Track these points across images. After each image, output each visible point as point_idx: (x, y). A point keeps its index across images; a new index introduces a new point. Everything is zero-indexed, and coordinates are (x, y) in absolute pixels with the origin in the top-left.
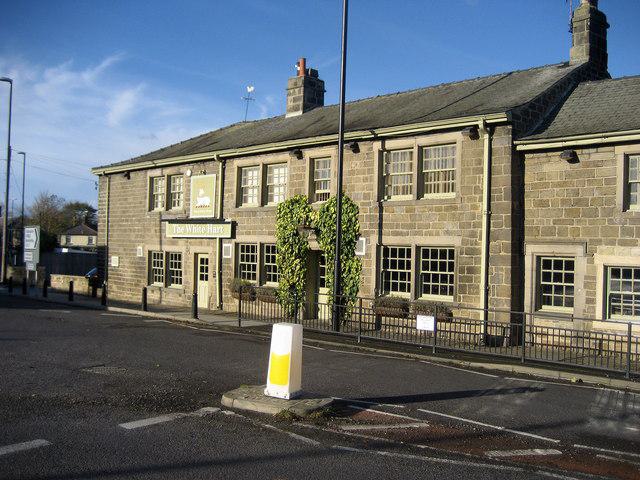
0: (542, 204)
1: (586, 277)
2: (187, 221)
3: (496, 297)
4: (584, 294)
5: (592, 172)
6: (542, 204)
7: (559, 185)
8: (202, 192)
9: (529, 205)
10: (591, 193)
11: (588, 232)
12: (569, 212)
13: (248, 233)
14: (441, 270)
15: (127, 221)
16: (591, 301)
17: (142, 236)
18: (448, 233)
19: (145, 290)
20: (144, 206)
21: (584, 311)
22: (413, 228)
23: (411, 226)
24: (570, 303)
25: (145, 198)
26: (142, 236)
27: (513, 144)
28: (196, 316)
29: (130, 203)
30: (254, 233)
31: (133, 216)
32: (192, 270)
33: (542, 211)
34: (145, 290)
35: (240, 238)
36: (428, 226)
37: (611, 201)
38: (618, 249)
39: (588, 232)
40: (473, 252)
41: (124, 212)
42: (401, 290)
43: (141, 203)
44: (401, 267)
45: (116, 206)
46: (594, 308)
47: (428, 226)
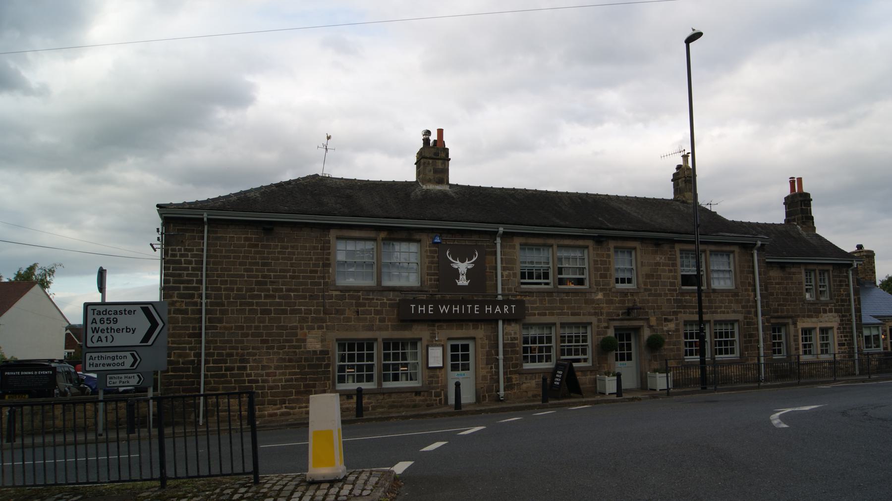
18: (734, 312)
36: (721, 307)
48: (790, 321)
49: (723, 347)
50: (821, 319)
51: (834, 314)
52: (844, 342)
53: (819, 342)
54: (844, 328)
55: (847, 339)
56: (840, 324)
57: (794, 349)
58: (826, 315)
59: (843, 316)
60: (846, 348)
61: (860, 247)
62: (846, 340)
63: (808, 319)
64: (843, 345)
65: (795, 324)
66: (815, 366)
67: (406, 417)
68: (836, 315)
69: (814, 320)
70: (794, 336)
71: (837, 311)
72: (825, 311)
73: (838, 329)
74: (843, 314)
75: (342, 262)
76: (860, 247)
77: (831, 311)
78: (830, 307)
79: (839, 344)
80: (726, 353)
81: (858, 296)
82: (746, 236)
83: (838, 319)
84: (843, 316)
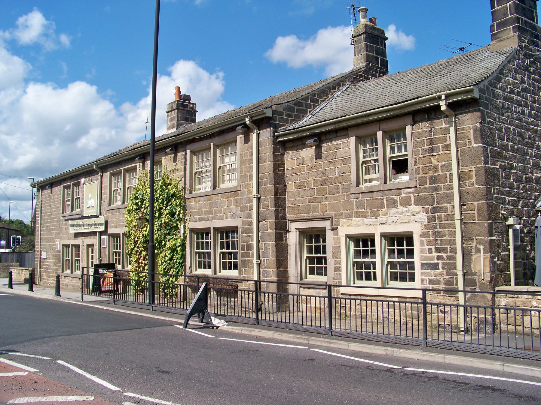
0: (301, 186)
1: (333, 248)
2: (83, 218)
3: (266, 269)
4: (333, 263)
5: (333, 154)
6: (301, 186)
7: (311, 168)
8: (90, 196)
9: (290, 187)
10: (333, 172)
11: (333, 208)
12: (319, 191)
13: (115, 227)
14: (315, 254)
15: (51, 222)
16: (338, 269)
17: (59, 234)
18: (233, 216)
19: (58, 277)
20: (60, 210)
21: (334, 279)
22: (212, 214)
23: (210, 213)
24: (412, 279)
25: (60, 204)
26: (59, 234)
27: (274, 135)
28: (58, 293)
29: (53, 208)
30: (119, 226)
31: (54, 218)
32: (85, 258)
33: (301, 192)
34: (58, 277)
35: (110, 231)
36: (220, 211)
37: (348, 179)
38: (356, 221)
39: (333, 208)
40: (249, 231)
41: (49, 215)
42: (366, 279)
43: (58, 207)
44: (317, 252)
45: (45, 210)
46: (340, 275)
47: (220, 211)
48: (327, 224)
49: (398, 271)
50: (382, 219)
51: (414, 208)
52: (436, 261)
53: (378, 259)
54: (436, 234)
55: (444, 255)
56: (426, 227)
57: (333, 269)
58: (393, 211)
59: (435, 210)
60: (441, 274)
61: (198, 111)
62: (439, 258)
63: (357, 220)
64: (435, 266)
65: (334, 229)
66: (146, 284)
67: (415, 353)
68: (419, 208)
69: (370, 220)
70: (334, 248)
71: (419, 201)
72: (393, 204)
73: (423, 235)
74: (436, 205)
75: (406, 181)
76: (198, 111)
77: (406, 202)
78: (403, 195)
79: (422, 264)
80: (319, 274)
81: (450, 172)
82: (246, 114)
83: (423, 217)
84: (435, 210)
